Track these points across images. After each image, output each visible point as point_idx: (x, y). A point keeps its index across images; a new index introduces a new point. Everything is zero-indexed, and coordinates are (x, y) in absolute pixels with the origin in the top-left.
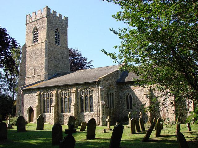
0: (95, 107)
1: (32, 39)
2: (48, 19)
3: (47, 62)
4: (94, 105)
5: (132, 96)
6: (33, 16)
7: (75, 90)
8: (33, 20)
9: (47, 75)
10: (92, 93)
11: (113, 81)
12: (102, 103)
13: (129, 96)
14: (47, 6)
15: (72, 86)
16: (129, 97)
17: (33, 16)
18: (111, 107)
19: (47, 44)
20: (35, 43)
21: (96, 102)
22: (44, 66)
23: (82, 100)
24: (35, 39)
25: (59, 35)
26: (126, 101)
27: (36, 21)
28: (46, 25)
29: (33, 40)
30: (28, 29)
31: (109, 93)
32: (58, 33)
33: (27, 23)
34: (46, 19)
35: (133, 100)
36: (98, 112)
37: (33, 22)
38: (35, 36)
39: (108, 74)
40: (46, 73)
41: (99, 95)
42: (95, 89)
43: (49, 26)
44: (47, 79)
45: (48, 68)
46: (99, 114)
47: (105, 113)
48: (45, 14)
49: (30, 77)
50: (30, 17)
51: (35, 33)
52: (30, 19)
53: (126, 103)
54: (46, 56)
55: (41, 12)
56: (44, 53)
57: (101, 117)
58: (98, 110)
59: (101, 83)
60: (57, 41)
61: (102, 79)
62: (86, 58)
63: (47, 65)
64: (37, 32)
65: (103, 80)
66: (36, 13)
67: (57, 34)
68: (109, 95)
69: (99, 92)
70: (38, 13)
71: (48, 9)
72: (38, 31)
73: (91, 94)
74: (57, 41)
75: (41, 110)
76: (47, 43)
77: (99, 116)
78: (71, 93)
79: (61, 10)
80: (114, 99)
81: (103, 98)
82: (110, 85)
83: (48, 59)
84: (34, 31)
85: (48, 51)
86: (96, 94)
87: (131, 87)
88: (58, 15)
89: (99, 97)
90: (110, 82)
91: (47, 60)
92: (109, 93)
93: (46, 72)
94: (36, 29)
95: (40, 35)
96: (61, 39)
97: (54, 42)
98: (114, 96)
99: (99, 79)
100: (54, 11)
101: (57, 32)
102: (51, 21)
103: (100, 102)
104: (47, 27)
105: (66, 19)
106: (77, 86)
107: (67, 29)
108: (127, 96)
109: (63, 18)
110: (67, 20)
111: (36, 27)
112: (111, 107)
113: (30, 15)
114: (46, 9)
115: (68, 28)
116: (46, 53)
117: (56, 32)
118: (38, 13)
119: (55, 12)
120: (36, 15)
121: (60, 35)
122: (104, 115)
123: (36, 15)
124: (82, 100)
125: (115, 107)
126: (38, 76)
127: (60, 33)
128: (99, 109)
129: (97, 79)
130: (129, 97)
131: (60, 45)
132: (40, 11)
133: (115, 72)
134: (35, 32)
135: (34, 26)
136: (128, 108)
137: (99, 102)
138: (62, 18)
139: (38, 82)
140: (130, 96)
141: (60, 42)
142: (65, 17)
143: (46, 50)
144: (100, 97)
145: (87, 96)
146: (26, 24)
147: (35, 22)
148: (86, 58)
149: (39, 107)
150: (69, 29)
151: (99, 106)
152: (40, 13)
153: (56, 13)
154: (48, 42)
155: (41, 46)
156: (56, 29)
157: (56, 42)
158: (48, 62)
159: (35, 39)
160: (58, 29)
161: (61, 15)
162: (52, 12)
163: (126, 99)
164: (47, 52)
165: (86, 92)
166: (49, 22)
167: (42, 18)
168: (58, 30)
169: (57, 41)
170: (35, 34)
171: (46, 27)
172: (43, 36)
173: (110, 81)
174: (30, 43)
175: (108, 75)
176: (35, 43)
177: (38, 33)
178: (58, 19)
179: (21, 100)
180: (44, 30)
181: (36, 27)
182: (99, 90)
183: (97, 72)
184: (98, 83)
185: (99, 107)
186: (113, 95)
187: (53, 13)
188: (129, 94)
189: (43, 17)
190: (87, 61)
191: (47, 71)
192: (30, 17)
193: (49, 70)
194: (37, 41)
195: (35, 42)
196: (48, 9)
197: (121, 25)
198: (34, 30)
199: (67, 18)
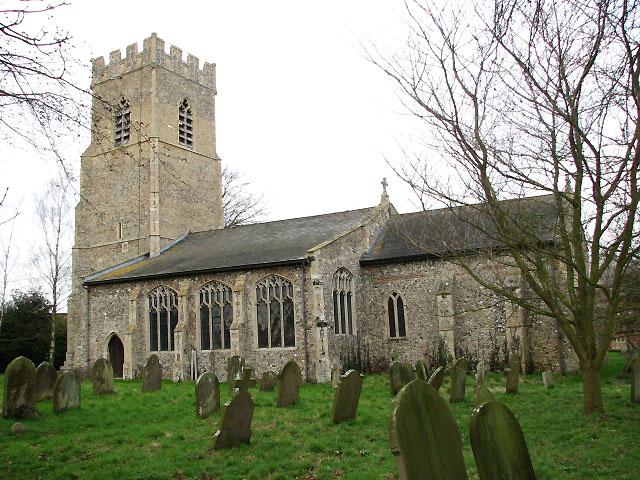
5: (404, 301)
13: (395, 299)
16: (395, 304)
26: (387, 314)
32: (189, 112)
47: (326, 348)
75: (142, 343)
80: (353, 310)
98: (353, 299)
107: (213, 100)
109: (184, 59)
125: (355, 333)
127: (194, 112)
130: (395, 304)
136: (393, 333)
140: (400, 301)
163: (387, 308)
173: (340, 258)
199: (214, 65)
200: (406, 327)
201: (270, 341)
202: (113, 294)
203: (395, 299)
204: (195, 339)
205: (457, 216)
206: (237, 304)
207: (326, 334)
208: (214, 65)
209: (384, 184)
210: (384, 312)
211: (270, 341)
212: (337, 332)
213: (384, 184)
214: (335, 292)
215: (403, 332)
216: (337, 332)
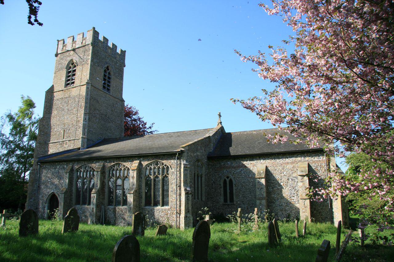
0: (172, 198)
1: (64, 79)
2: (93, 48)
3: (87, 119)
4: (170, 193)
5: (234, 181)
6: (69, 42)
7: (137, 165)
8: (69, 47)
9: (86, 140)
10: (167, 171)
11: (202, 154)
12: (185, 190)
13: (228, 180)
14: (94, 28)
15: (130, 158)
16: (228, 183)
17: (69, 42)
18: (198, 198)
19: (90, 88)
20: (69, 87)
21: (175, 188)
22: (81, 124)
23: (148, 185)
24: (69, 81)
25: (110, 77)
26: (222, 189)
27: (74, 50)
28: (90, 57)
29: (66, 82)
30: (59, 63)
31: (196, 174)
32: (109, 73)
33: (59, 53)
34: (91, 48)
35: (234, 188)
36: (178, 206)
37: (68, 51)
38: (69, 78)
39: (196, 140)
40: (84, 137)
41: (180, 176)
42: (172, 163)
43: (95, 60)
44: (86, 146)
45: (88, 128)
46: (180, 210)
47: (190, 208)
48: (89, 39)
49: (55, 141)
50: (64, 43)
51: (69, 78)
52: (63, 47)
53: (222, 193)
54: (86, 107)
55: (83, 37)
56: (83, 104)
57: (183, 215)
58: (178, 203)
59: (185, 154)
60: (106, 86)
61: (187, 148)
62: (145, 122)
63: (87, 123)
64: (74, 69)
65: (188, 150)
66: (74, 38)
67: (107, 74)
68: (196, 178)
69: (180, 170)
70: (79, 39)
71: (96, 34)
72: (75, 66)
73: (165, 173)
74: (107, 86)
75: (71, 200)
76: (90, 87)
77: (180, 214)
78: (128, 169)
79: (116, 39)
80: (203, 186)
81: (188, 181)
82: (198, 161)
83: (89, 114)
84: (68, 67)
85: (90, 100)
86: (176, 173)
87: (245, 163)
89: (180, 180)
90: (197, 156)
91: (87, 115)
92: (196, 174)
93: (84, 134)
94: (72, 64)
95: (78, 73)
96: (113, 83)
97: (101, 88)
98: (203, 179)
99: (182, 147)
101: (108, 72)
102: (98, 53)
103: (183, 189)
104: (92, 61)
105: (123, 52)
106: (141, 159)
107: (123, 69)
108: (225, 181)
109: (119, 51)
110: (124, 56)
111: (72, 60)
112: (198, 198)
113: (64, 40)
114: (91, 33)
116: (86, 103)
117: (105, 71)
118: (79, 39)
121: (112, 77)
122: (188, 212)
124: (148, 185)
125: (204, 199)
126: (70, 140)
127: (112, 73)
128: (180, 201)
129: (179, 147)
130: (228, 183)
131: (111, 92)
132: (82, 35)
133: (205, 138)
134: (70, 68)
135: (69, 59)
136: (225, 200)
137: (180, 189)
138: (116, 50)
139: (70, 150)
140: (231, 181)
141: (111, 88)
142: (121, 50)
143: (86, 99)
144: (182, 179)
145: (157, 177)
146: (57, 55)
147: (72, 52)
148: (145, 122)
149: (154, 157)
151: (180, 195)
152: (81, 39)
154: (90, 84)
155: (80, 90)
156: (106, 66)
157: (104, 87)
158: (89, 119)
159: (69, 81)
160: (109, 68)
161: (115, 46)
162: (101, 38)
163: (222, 185)
164: (88, 101)
165: (156, 170)
167: (84, 46)
168: (108, 69)
169: (107, 86)
170: (70, 72)
171: (90, 61)
172: (83, 74)
173: (198, 153)
174: (60, 86)
175: (196, 142)
176: (68, 86)
177: (75, 71)
178: (109, 51)
179: (36, 178)
180: (86, 65)
181: (72, 60)
182: (180, 167)
183: (172, 139)
184: (179, 154)
185: (180, 198)
186: (201, 177)
188: (228, 177)
189: (86, 44)
190: (147, 126)
191: (86, 134)
192: (64, 43)
193: (89, 131)
195: (68, 84)
196: (96, 34)
197: (15, 235)
198: (68, 65)
199: (125, 51)
200: (234, 197)
201: (152, 202)
202: (55, 169)
203: (228, 180)
204: (104, 199)
205: (70, 175)
206: (133, 177)
207: (190, 199)
208: (125, 51)
209: (220, 116)
210: (221, 188)
211: (152, 202)
212: (195, 199)
213: (220, 116)
214: (194, 174)
215: (232, 200)
216: (195, 199)
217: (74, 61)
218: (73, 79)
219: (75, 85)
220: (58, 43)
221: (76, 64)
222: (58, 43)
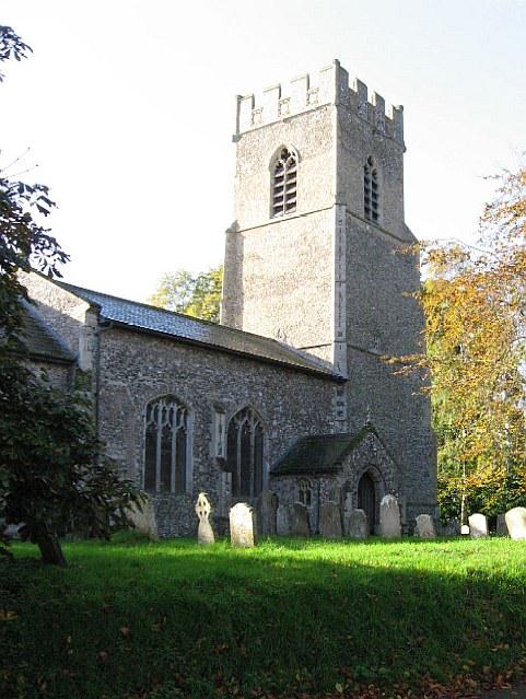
6: (268, 102)
14: (337, 62)
17: (268, 102)
24: (283, 197)
25: (377, 193)
38: (279, 195)
48: (328, 94)
51: (279, 195)
52: (253, 115)
67: (370, 177)
71: (342, 74)
74: (371, 212)
79: (385, 85)
88: (371, 99)
100: (359, 81)
113: (253, 98)
114: (333, 72)
115: (406, 157)
119: (362, 86)
120: (282, 101)
123: (282, 101)
146: (236, 138)
150: (410, 161)
153: (348, 74)
159: (283, 197)
162: (352, 85)
166: (344, 129)
170: (281, 179)
172: (319, 178)
177: (294, 175)
187: (356, 90)
193: (350, 320)
194: (290, 206)
196: (342, 74)
198: (275, 158)
199: (402, 107)
217: (290, 150)
218: (290, 186)
219: (299, 210)
220: (239, 103)
221: (296, 158)
222: (239, 103)
